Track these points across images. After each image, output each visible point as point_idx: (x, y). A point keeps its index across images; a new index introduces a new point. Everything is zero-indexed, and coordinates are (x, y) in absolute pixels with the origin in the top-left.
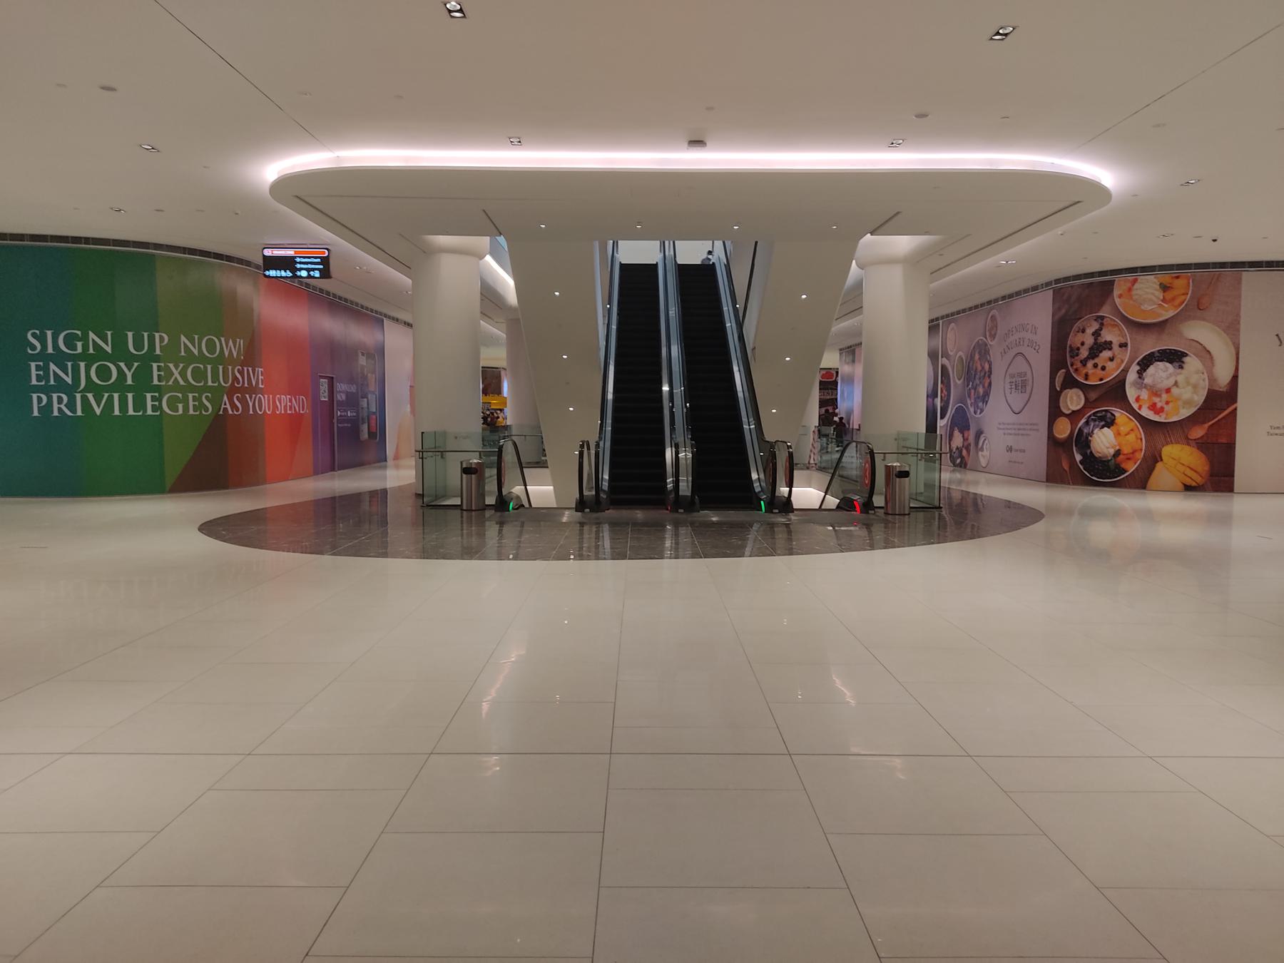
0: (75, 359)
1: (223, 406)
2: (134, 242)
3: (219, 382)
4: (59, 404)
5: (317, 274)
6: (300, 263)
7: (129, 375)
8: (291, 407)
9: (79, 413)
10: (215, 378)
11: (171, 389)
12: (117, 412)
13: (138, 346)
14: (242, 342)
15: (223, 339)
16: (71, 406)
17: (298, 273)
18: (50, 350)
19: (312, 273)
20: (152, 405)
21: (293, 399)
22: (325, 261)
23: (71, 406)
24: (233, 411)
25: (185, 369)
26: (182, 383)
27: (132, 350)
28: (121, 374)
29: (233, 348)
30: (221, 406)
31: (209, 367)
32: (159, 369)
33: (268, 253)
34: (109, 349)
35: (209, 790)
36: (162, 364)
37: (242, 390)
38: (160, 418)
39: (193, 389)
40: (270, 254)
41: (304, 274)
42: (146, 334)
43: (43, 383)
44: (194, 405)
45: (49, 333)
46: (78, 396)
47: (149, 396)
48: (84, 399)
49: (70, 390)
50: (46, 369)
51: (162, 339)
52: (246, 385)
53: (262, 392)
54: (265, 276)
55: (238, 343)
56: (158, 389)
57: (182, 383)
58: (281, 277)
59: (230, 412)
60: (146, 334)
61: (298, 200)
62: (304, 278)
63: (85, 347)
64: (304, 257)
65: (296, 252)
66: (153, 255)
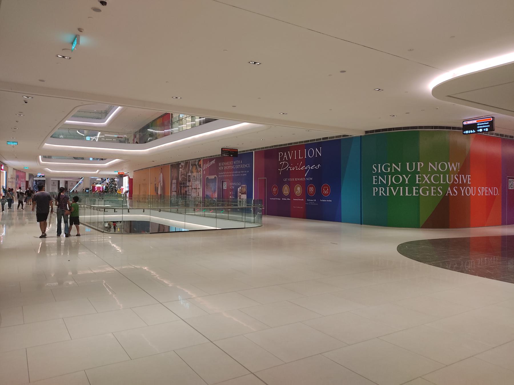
0: (387, 174)
1: (448, 192)
2: (425, 127)
3: (446, 182)
4: (381, 191)
5: (487, 130)
6: (479, 126)
7: (407, 180)
8: (487, 193)
9: (388, 195)
10: (444, 180)
11: (424, 185)
12: (401, 195)
13: (411, 168)
14: (459, 164)
15: (449, 163)
16: (385, 192)
17: (478, 131)
18: (379, 171)
19: (484, 129)
20: (433, 191)
21: (489, 189)
22: (491, 123)
23: (385, 192)
24: (453, 194)
25: (430, 177)
26: (429, 182)
27: (409, 170)
28: (404, 180)
29: (454, 167)
30: (447, 192)
31: (442, 175)
32: (419, 177)
33: (465, 123)
34: (399, 170)
35: (420, 377)
36: (421, 175)
37: (458, 185)
38: (418, 197)
39: (433, 185)
40: (466, 124)
41: (481, 130)
42: (414, 163)
43: (377, 184)
44: (487, 192)
45: (379, 165)
46: (388, 188)
47: (414, 188)
48: (390, 189)
49: (385, 186)
50: (378, 178)
51: (421, 165)
52: (460, 183)
53: (470, 186)
54: (464, 134)
55: (457, 164)
56: (418, 185)
57: (429, 182)
58: (471, 133)
59: (451, 195)
60: (414, 163)
61: (449, 97)
62: (480, 132)
63: (391, 170)
64: (481, 123)
65: (477, 121)
66: (419, 131)
